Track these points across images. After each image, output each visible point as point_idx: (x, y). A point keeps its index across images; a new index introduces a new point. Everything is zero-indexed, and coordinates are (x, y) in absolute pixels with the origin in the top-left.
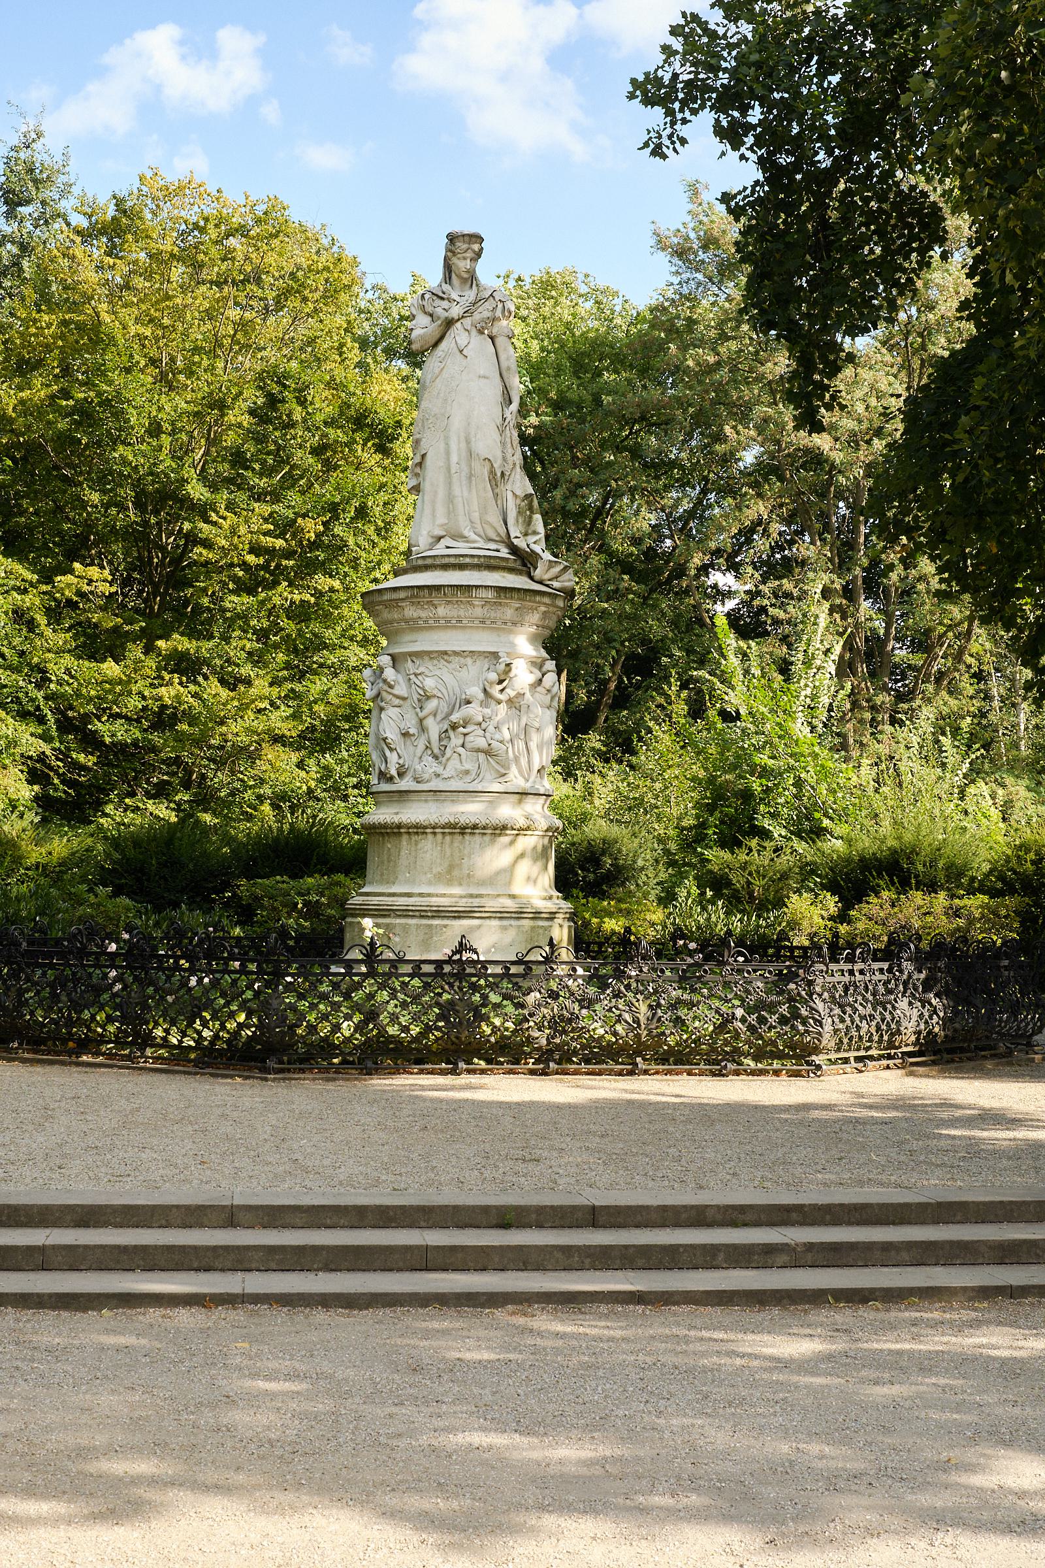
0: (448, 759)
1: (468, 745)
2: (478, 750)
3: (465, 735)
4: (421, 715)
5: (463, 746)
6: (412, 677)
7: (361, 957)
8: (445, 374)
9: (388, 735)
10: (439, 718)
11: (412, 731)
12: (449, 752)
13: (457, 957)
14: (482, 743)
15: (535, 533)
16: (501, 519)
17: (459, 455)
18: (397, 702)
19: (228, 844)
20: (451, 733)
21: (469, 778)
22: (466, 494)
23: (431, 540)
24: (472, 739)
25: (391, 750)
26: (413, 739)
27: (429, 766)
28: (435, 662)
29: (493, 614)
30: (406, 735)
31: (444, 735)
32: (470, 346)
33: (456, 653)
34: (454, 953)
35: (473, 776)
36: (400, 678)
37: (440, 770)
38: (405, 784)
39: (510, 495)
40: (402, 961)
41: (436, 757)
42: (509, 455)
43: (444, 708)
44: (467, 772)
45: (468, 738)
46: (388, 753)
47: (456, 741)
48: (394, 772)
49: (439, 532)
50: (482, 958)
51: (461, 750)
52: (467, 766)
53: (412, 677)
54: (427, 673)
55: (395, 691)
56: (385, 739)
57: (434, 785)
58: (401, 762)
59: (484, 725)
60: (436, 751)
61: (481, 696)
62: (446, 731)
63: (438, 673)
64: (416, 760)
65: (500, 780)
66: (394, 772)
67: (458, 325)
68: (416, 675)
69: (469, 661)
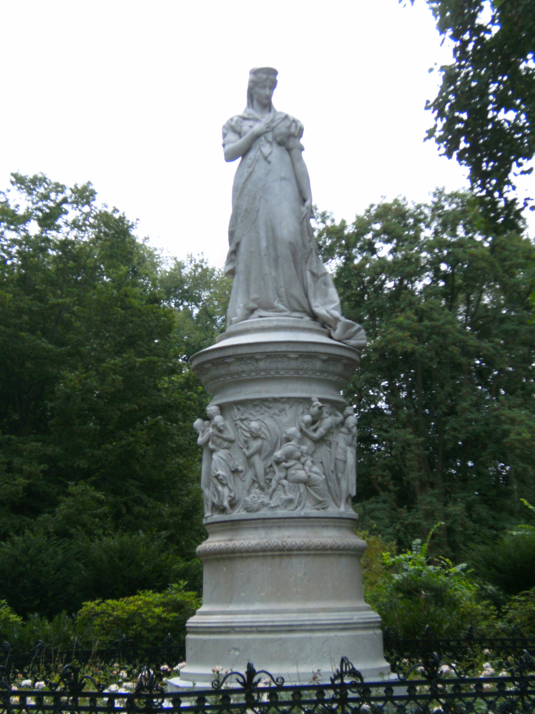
0: (274, 491)
1: (291, 478)
2: (299, 481)
3: (287, 468)
4: (248, 453)
5: (286, 478)
6: (238, 422)
7: (238, 686)
8: (254, 177)
9: (220, 472)
10: (264, 455)
11: (240, 468)
12: (274, 484)
13: (337, 682)
14: (302, 474)
15: (332, 302)
16: (304, 295)
17: (268, 241)
18: (226, 444)
19: (434, 248)
20: (276, 468)
21: (292, 507)
22: (273, 274)
23: (246, 312)
24: (293, 472)
25: (223, 485)
26: (241, 475)
27: (255, 497)
28: (258, 409)
29: (306, 366)
30: (235, 472)
31: (269, 470)
32: (272, 155)
33: (276, 400)
34: (336, 677)
35: (296, 502)
36: (228, 424)
37: (266, 500)
38: (238, 513)
39: (308, 274)
40: (281, 688)
41: (262, 489)
42: (307, 242)
43: (267, 447)
44: (291, 501)
45: (292, 471)
46: (220, 488)
47: (279, 474)
48: (226, 503)
49: (252, 305)
50: (366, 680)
51: (284, 482)
52: (290, 496)
53: (238, 422)
54: (251, 417)
55: (225, 435)
56: (217, 477)
57: (264, 513)
58: (232, 495)
59: (303, 460)
60: (262, 484)
61: (299, 435)
62: (271, 466)
63: (260, 417)
64: (245, 492)
65: (318, 506)
66: (226, 503)
67: (263, 138)
68: (242, 420)
69: (287, 406)
